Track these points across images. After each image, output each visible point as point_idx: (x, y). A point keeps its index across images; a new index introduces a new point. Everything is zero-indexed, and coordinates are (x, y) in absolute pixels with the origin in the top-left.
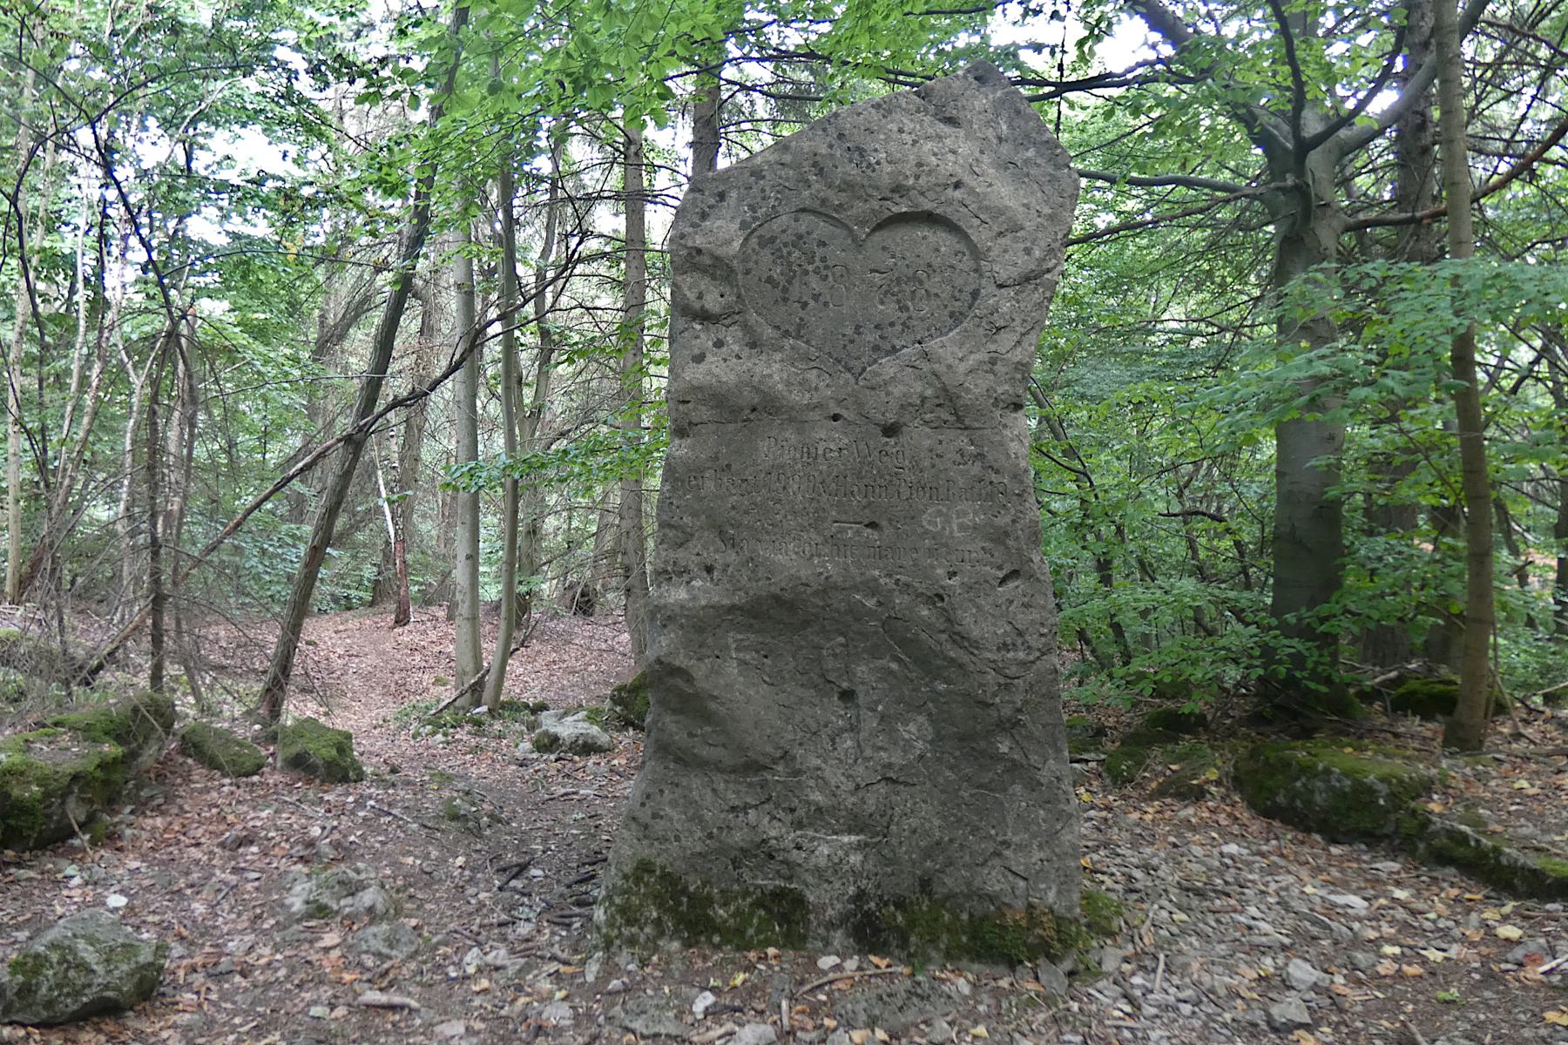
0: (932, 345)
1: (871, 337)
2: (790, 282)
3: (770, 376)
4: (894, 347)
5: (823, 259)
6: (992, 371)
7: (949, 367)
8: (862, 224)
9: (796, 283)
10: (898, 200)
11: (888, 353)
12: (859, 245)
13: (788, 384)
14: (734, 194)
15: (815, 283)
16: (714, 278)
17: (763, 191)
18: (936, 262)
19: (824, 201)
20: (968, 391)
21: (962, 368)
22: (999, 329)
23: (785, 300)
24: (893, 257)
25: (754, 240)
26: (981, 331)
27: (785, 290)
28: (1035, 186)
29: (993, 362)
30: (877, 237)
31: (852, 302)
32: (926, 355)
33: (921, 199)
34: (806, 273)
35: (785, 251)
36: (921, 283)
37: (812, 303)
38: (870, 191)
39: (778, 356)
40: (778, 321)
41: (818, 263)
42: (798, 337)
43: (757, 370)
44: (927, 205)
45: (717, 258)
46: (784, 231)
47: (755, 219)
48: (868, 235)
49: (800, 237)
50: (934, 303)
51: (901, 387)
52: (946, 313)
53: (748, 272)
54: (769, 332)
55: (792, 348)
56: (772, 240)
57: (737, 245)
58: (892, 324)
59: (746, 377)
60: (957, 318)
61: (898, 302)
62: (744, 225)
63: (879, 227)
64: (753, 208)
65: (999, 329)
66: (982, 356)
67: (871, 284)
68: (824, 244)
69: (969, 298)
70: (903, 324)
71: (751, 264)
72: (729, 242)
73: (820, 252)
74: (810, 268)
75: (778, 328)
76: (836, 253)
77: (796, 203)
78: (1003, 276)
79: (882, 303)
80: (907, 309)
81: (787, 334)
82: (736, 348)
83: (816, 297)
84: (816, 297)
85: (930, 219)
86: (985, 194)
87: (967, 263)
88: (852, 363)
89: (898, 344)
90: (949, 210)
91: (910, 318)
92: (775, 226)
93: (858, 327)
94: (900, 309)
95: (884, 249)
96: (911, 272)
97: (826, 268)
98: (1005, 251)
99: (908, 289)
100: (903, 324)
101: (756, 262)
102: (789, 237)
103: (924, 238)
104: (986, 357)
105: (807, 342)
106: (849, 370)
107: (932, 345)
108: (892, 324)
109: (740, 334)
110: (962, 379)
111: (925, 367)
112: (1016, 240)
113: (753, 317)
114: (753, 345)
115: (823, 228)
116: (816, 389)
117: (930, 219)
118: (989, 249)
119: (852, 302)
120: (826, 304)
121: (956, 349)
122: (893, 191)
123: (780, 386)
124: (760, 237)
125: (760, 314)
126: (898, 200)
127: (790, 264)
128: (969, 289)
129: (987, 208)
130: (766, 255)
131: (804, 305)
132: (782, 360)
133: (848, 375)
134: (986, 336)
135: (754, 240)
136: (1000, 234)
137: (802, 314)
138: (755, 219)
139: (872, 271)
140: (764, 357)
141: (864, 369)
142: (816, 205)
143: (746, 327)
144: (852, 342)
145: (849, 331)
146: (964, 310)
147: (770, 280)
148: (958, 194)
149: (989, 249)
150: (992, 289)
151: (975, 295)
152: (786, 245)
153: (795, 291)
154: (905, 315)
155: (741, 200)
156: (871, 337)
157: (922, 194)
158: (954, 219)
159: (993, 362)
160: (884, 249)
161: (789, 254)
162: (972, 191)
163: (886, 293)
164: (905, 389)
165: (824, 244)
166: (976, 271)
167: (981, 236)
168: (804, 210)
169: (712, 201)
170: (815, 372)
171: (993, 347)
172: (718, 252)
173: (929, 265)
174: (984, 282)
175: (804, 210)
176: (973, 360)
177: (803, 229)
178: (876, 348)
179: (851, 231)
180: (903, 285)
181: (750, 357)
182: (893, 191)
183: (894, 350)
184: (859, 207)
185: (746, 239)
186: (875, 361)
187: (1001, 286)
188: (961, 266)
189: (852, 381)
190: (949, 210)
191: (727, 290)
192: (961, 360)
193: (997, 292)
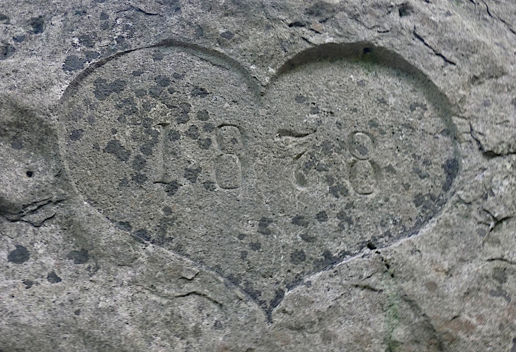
0: (397, 248)
1: (288, 238)
2: (147, 150)
3: (112, 310)
4: (327, 254)
5: (203, 115)
6: (500, 292)
7: (432, 286)
8: (262, 60)
9: (159, 151)
10: (319, 26)
11: (319, 265)
12: (259, 92)
13: (145, 324)
14: (57, 21)
15: (189, 151)
16: (16, 144)
17: (104, 16)
18: (384, 119)
19: (201, 30)
20: (469, 328)
21: (452, 287)
22: (499, 222)
23: (139, 179)
24: (315, 111)
25: (87, 88)
26: (472, 225)
27: (140, 163)
28: (502, 25)
29: (501, 276)
30: (287, 82)
31: (252, 181)
32: (386, 267)
33: (353, 25)
34: (174, 136)
35: (139, 103)
36: (363, 150)
37: (185, 184)
38: (274, 13)
39: (126, 274)
40: (126, 213)
41: (193, 120)
42: (162, 241)
43: (88, 300)
44: (364, 34)
45: (23, 111)
46: (137, 74)
47: (89, 56)
48: (274, 78)
49: (164, 82)
50: (388, 181)
51: (37, 128)
52: (409, 197)
53: (75, 135)
54: (110, 233)
55: (152, 260)
56: (118, 86)
57: (57, 91)
58: (322, 216)
59: (67, 315)
60: (428, 205)
61: (329, 180)
62: (70, 64)
63: (290, 66)
64: (86, 40)
65: (499, 222)
66: (478, 266)
67: (283, 153)
68: (203, 93)
69: (441, 172)
70: (341, 215)
71: (81, 124)
72: (44, 87)
73: (196, 104)
74: (182, 128)
75: (127, 225)
76: (226, 103)
77: (155, 33)
78: (491, 139)
79: (302, 181)
80: (345, 192)
81: (142, 236)
82: (50, 262)
83: (192, 175)
84: (192, 175)
85: (368, 55)
86: (445, 24)
87: (431, 121)
88: (259, 284)
89: (335, 248)
90: (397, 42)
91: (350, 205)
92: (125, 64)
93: (264, 223)
94: (334, 191)
95: (300, 99)
96: (345, 134)
97: (208, 128)
98: (486, 104)
99: (343, 159)
100: (341, 215)
101: (91, 120)
102: (146, 83)
103: (361, 83)
104: (489, 268)
105: (179, 249)
106: (254, 295)
107: (397, 248)
108: (322, 216)
109: (59, 238)
110: (456, 306)
111: (389, 287)
112: (497, 89)
113: (82, 208)
114: (82, 256)
115: (200, 71)
116: (197, 332)
117: (368, 55)
118: (463, 100)
119: (252, 181)
120: (209, 185)
121: (437, 255)
122: (310, 13)
123: (130, 330)
124: (98, 82)
125: (94, 203)
126: (319, 26)
127: (147, 123)
128: (441, 159)
129: (451, 44)
130: (108, 109)
131: (172, 188)
132: (134, 282)
133: (254, 306)
134: (481, 233)
135: (87, 88)
136: (475, 80)
137: (168, 201)
138: (89, 56)
139: (283, 133)
140: (100, 277)
141: (280, 295)
142: (190, 35)
143: (69, 226)
144: (256, 246)
145: (250, 229)
146: (438, 191)
147: (113, 147)
148: (407, 22)
149: (463, 100)
150: (477, 158)
151: (452, 168)
152: (140, 93)
153: (157, 165)
154: (342, 201)
155: (67, 30)
156: (288, 238)
157: (355, 18)
158: (406, 55)
159: (501, 276)
160: (300, 99)
161: (146, 107)
162: (425, 19)
163: (308, 166)
164: (357, 328)
165: (203, 93)
166: (446, 132)
167: (447, 80)
168: (169, 43)
169: (21, 31)
170: (192, 300)
171: (496, 252)
172: (26, 101)
173: (373, 124)
174: (463, 148)
175: (169, 43)
176: (468, 272)
177: (168, 71)
178: (298, 257)
179: (245, 72)
180: (332, 156)
181: (75, 277)
182: (310, 13)
183: (329, 260)
184: (257, 38)
185: (75, 85)
186: (298, 280)
187: (490, 155)
188: (422, 125)
189: (261, 315)
190: (397, 42)
191: (39, 165)
192: (448, 273)
193: (485, 164)
